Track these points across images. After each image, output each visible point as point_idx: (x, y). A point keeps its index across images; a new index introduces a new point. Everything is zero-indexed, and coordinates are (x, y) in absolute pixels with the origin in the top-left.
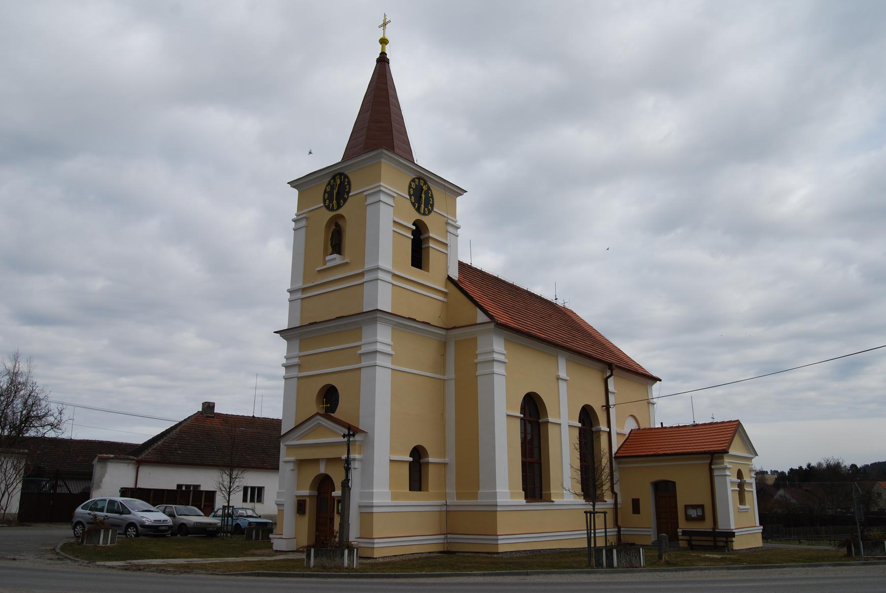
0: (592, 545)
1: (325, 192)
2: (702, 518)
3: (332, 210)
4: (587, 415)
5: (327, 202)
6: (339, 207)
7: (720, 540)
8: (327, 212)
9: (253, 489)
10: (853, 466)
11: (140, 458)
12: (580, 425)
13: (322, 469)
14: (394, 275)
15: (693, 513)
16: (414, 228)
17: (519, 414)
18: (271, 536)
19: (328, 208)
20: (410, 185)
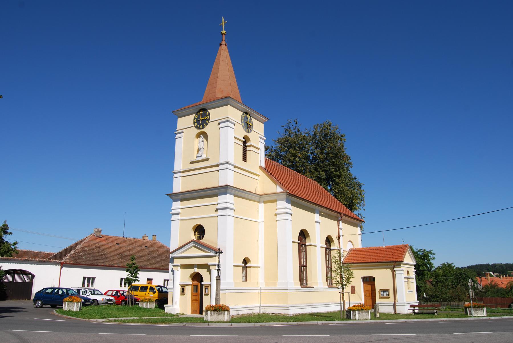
0: (343, 309)
1: (195, 118)
2: (388, 297)
3: (199, 129)
4: (329, 240)
5: (196, 124)
6: (203, 127)
7: (415, 255)
8: (196, 130)
9: (89, 278)
10: (488, 264)
11: (62, 261)
12: (326, 246)
13: (196, 270)
14: (235, 167)
15: (385, 294)
16: (244, 140)
17: (297, 241)
18: (165, 306)
19: (196, 127)
20: (242, 117)
